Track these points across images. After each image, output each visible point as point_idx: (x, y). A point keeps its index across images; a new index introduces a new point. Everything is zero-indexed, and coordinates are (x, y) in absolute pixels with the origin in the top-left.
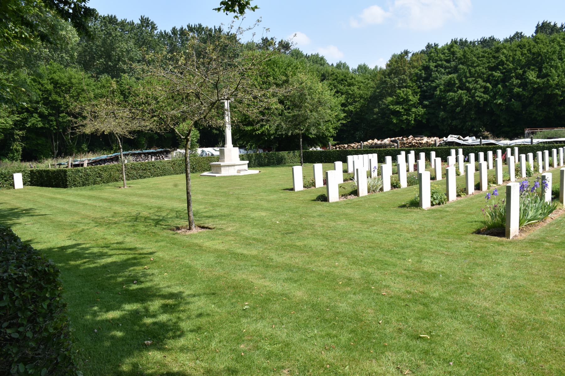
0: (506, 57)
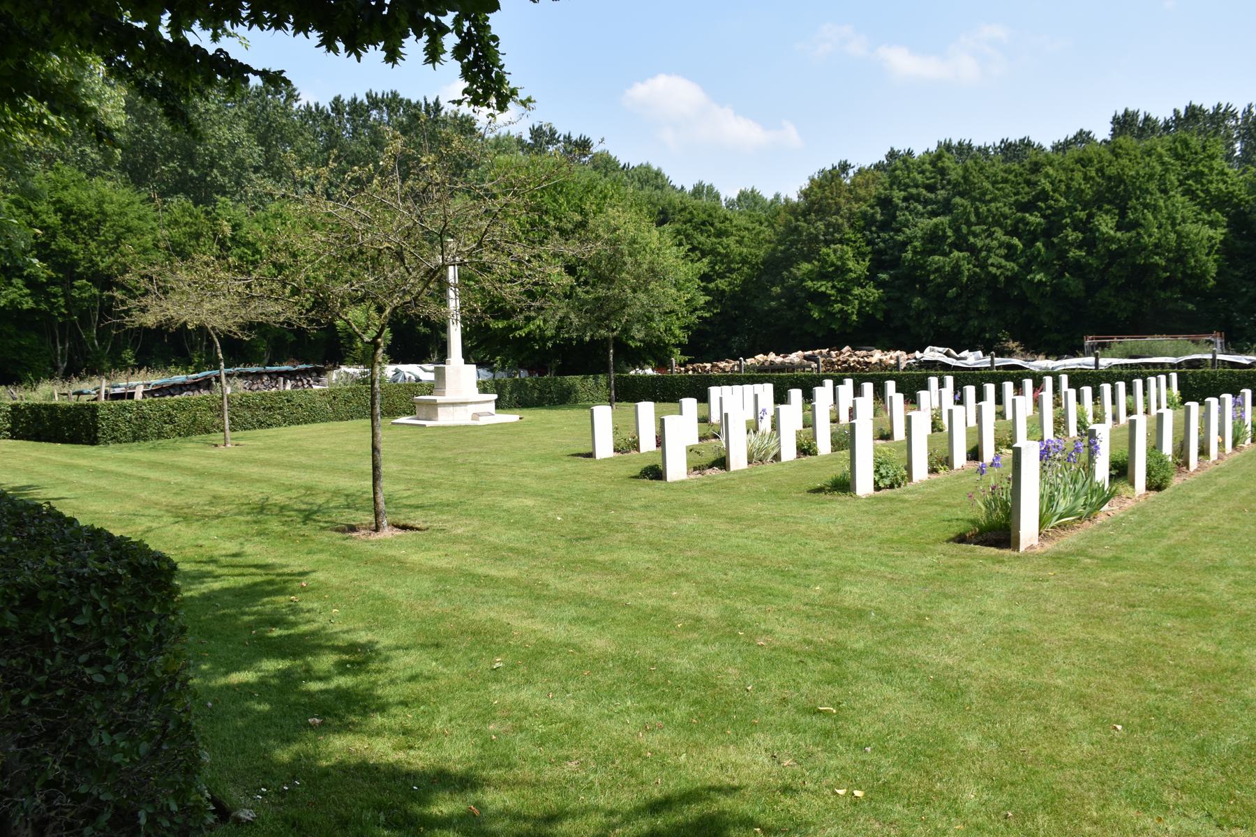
0: (1052, 183)
